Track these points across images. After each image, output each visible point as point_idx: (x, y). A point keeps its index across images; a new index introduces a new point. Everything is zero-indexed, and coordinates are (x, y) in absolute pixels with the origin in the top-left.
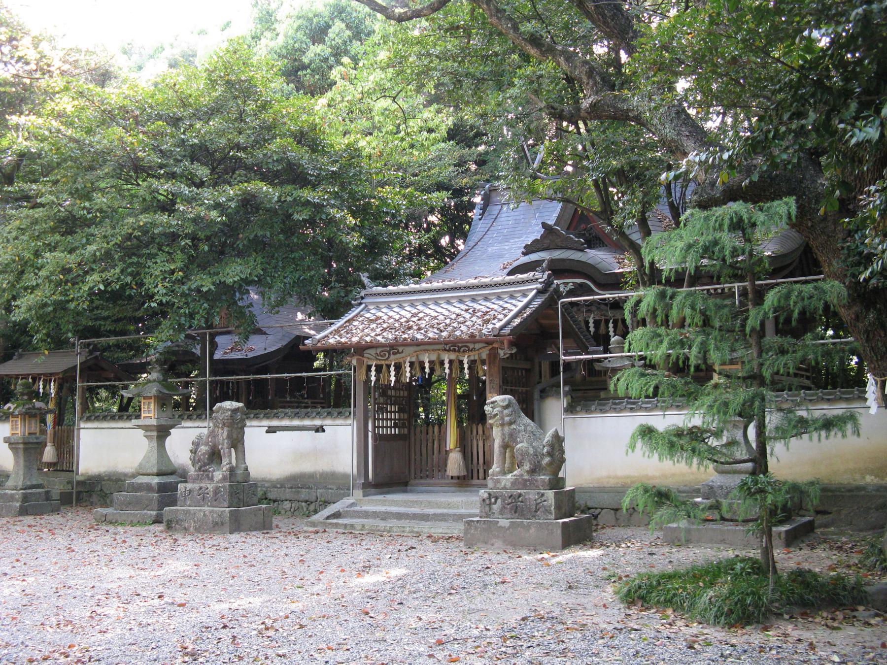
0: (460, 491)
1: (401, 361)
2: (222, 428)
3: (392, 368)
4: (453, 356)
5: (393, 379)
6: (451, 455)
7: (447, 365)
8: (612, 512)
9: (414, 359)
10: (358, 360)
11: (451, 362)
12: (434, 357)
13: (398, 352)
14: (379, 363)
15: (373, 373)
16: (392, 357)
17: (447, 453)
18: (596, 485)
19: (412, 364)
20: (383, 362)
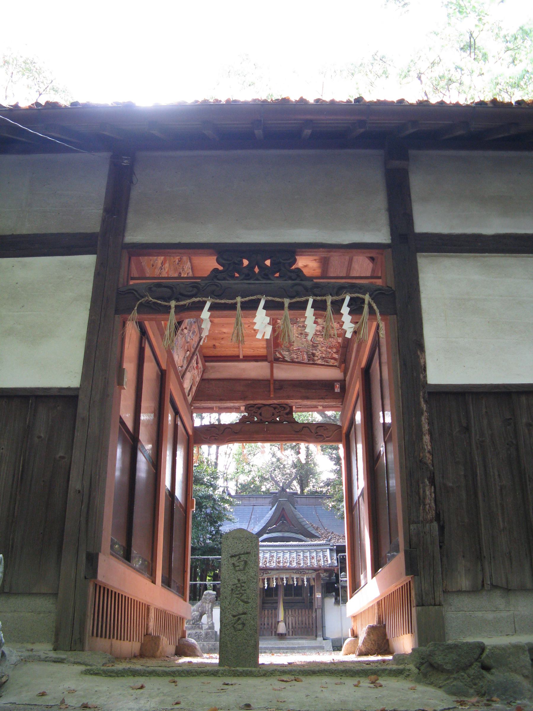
1: (271, 577)
2: (209, 603)
3: (266, 580)
4: (298, 576)
5: (266, 585)
6: (280, 623)
7: (295, 580)
9: (277, 577)
12: (288, 576)
13: (268, 573)
15: (266, 583)
16: (265, 575)
17: (278, 622)
19: (276, 579)
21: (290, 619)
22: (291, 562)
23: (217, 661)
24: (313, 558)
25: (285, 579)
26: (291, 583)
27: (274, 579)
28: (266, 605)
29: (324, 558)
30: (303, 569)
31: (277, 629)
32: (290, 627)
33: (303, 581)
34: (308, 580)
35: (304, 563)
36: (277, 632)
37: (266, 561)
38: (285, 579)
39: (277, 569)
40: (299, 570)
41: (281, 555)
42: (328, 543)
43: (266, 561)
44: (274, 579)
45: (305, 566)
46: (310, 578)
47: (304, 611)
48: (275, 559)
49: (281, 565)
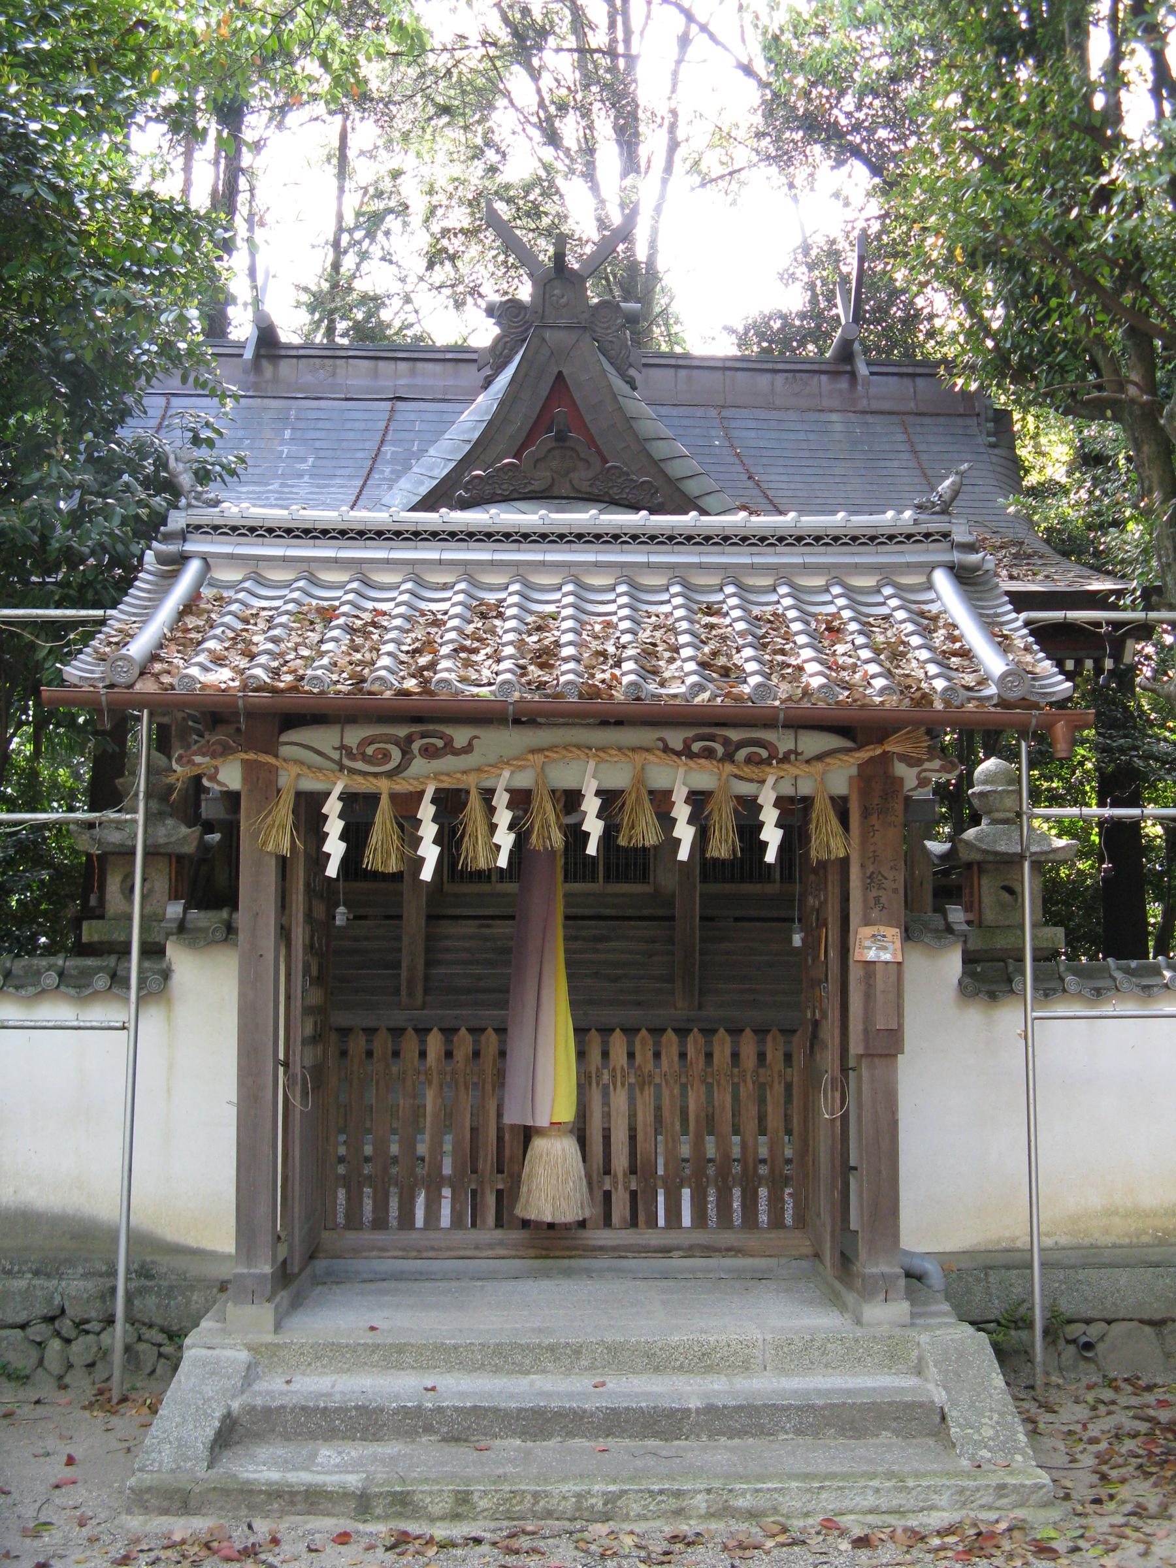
0: (547, 1274)
1: (471, 782)
3: (427, 811)
4: (704, 777)
5: (430, 853)
6: (539, 1145)
7: (681, 812)
8: (1148, 1330)
9: (524, 780)
10: (249, 768)
11: (698, 800)
12: (619, 777)
13: (449, 748)
14: (362, 785)
16: (419, 765)
17: (528, 1134)
18: (1064, 1240)
19: (521, 800)
20: (384, 786)
21: (619, 1100)
22: (649, 652)
23: (422, 877)
24: (834, 630)
25: (591, 805)
26: (648, 834)
27: (501, 799)
28: (448, 928)
29: (926, 632)
30: (769, 721)
31: (516, 1181)
32: (620, 1161)
33: (749, 830)
34: (795, 813)
35: (769, 669)
36: (520, 1212)
37: (428, 645)
38: (591, 805)
39: (521, 718)
40: (718, 729)
41: (559, 602)
42: (936, 525)
43: (428, 645)
44: (501, 799)
45: (784, 690)
46: (807, 802)
47: (722, 1046)
48: (507, 630)
49: (566, 674)
